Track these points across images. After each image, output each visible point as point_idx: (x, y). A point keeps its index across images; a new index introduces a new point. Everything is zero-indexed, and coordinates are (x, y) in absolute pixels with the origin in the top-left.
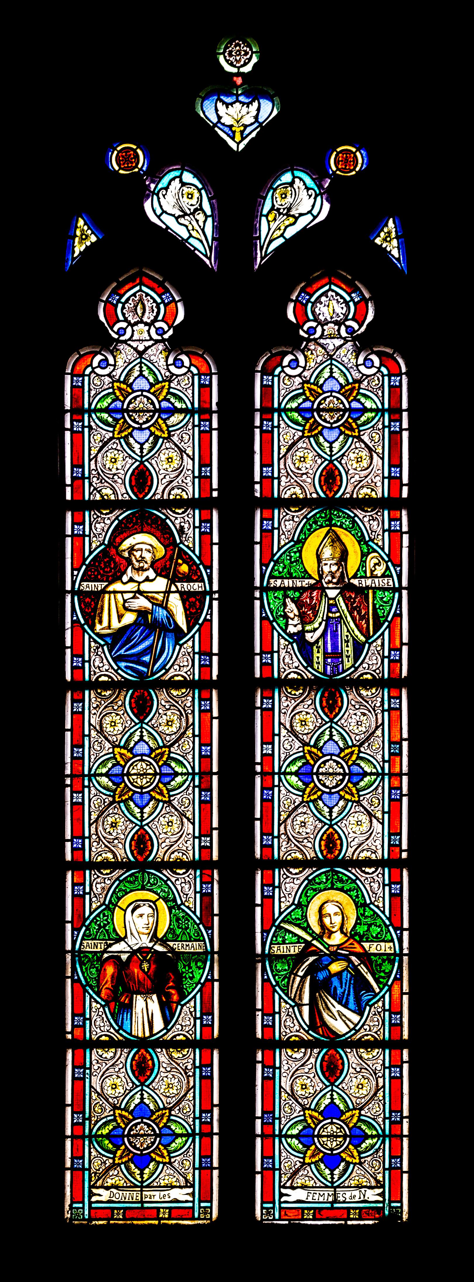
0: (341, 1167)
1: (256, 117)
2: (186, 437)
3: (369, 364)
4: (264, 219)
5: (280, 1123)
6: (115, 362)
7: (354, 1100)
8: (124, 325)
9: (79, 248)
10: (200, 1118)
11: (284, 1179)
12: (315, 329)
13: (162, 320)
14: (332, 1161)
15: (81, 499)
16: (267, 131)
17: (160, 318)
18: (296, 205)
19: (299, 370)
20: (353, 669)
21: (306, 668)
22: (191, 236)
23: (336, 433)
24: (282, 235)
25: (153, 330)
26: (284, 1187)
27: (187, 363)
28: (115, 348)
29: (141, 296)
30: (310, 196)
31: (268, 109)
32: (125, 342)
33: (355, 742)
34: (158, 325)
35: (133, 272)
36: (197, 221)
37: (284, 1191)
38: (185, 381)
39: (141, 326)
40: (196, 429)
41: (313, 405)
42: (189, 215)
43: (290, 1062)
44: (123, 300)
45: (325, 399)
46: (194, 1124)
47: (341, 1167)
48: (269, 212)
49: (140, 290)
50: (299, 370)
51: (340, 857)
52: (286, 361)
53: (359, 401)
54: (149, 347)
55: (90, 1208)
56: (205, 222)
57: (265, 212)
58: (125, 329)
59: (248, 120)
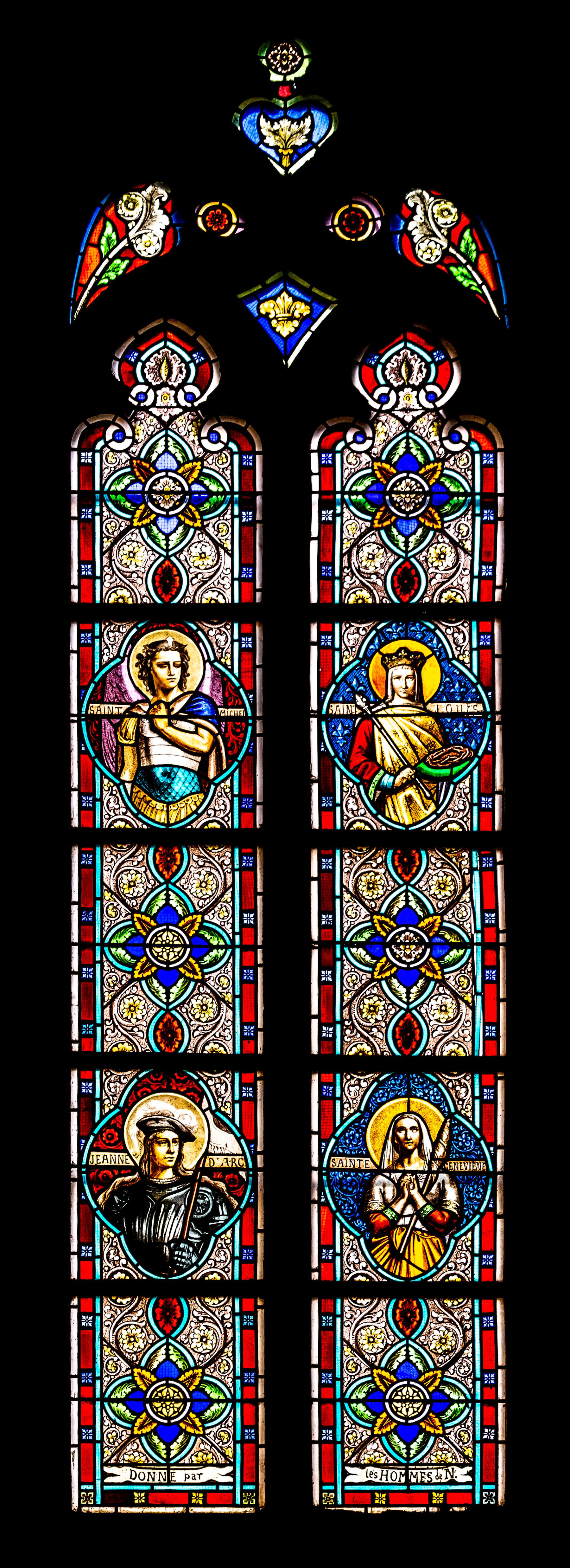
1: (309, 136)
2: (464, 529)
3: (214, 437)
5: (342, 1384)
7: (196, 1356)
11: (108, 1453)
12: (145, 394)
14: (408, 1431)
15: (91, 601)
17: (190, 380)
20: (434, 816)
21: (375, 816)
23: (174, 522)
25: (181, 394)
26: (107, 1464)
27: (465, 438)
28: (133, 417)
29: (406, 356)
31: (321, 127)
34: (188, 389)
35: (155, 324)
37: (107, 1469)
39: (167, 389)
43: (354, 1309)
44: (143, 358)
45: (158, 479)
51: (181, 1050)
52: (109, 435)
53: (201, 483)
54: (176, 416)
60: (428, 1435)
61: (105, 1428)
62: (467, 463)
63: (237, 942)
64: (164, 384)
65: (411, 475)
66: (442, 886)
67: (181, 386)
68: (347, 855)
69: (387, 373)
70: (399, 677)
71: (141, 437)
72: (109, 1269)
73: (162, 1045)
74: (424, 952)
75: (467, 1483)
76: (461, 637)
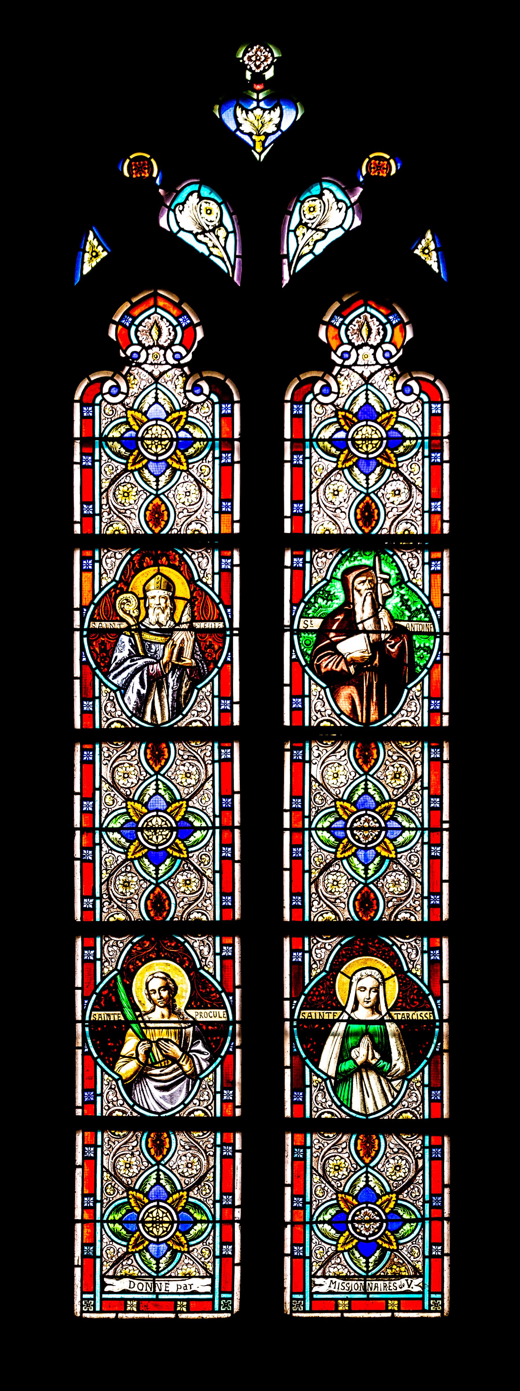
0: (377, 1254)
1: (278, 126)
4: (291, 234)
5: (102, 1207)
6: (339, 389)
8: (348, 348)
9: (87, 269)
10: (221, 1201)
13: (390, 342)
16: (286, 140)
17: (177, 341)
18: (323, 218)
19: (121, 397)
22: (211, 253)
23: (162, 466)
24: (311, 251)
25: (169, 354)
27: (416, 390)
29: (366, 319)
30: (340, 209)
32: (349, 367)
33: (184, 796)
34: (175, 349)
36: (218, 237)
38: (206, 409)
40: (217, 462)
41: (347, 435)
42: (209, 231)
46: (214, 1207)
47: (377, 1254)
48: (297, 227)
49: (155, 312)
50: (121, 397)
51: (377, 918)
52: (317, 389)
53: (187, 431)
54: (166, 372)
55: (312, 1299)
56: (226, 238)
57: (292, 227)
58: (349, 353)
59: (270, 128)
60: (384, 1251)
61: (313, 1245)
62: (417, 411)
63: (217, 824)
64: (366, 344)
65: (370, 423)
66: (188, 775)
67: (379, 345)
68: (314, 749)
69: (349, 333)
70: (153, 598)
71: (344, 390)
72: (109, 1108)
73: (360, 914)
74: (380, 833)
75: (418, 1293)
76: (415, 562)
